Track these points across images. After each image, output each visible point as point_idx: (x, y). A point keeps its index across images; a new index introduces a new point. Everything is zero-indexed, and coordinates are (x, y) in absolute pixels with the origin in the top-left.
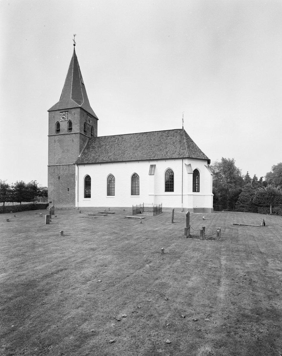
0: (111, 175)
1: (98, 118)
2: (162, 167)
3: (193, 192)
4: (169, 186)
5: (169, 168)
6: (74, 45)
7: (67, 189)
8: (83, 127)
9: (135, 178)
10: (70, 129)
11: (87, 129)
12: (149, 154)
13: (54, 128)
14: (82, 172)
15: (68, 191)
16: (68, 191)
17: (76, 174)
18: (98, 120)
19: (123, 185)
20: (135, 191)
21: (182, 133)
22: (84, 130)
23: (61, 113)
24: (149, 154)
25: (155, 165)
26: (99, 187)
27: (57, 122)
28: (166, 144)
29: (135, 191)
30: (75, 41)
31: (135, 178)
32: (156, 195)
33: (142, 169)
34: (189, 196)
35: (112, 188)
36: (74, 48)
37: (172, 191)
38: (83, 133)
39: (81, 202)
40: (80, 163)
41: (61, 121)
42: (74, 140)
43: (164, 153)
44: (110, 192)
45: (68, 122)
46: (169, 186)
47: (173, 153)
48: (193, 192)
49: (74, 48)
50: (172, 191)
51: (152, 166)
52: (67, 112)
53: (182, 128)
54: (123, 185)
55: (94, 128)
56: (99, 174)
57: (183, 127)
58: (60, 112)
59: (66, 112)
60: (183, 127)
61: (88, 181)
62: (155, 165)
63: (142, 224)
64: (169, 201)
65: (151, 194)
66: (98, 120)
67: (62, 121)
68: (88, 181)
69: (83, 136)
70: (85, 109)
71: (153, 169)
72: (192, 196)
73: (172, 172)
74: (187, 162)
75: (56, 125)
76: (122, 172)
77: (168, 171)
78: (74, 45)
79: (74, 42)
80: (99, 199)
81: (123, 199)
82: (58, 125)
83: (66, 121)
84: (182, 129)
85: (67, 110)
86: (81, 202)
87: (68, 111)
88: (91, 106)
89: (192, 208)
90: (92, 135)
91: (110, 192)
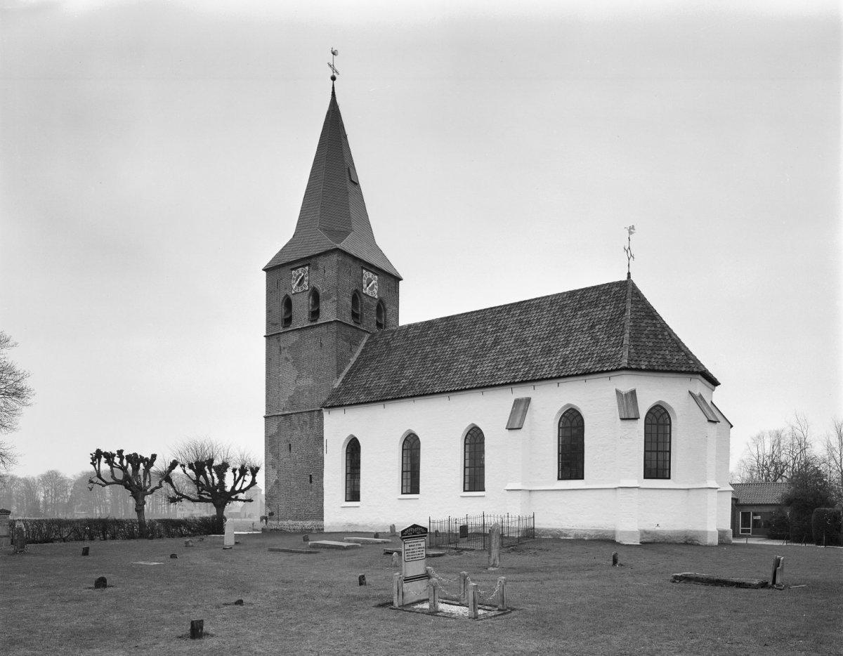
0: (412, 434)
1: (402, 274)
2: (548, 402)
3: (645, 478)
4: (571, 463)
5: (568, 405)
6: (333, 78)
8: (350, 303)
9: (474, 440)
10: (315, 314)
11: (362, 309)
12: (512, 368)
13: (280, 310)
14: (338, 427)
15: (311, 482)
16: (311, 482)
17: (467, 454)
18: (398, 279)
20: (474, 480)
22: (353, 312)
23: (293, 272)
24: (512, 368)
25: (528, 400)
26: (381, 467)
27: (284, 297)
28: (570, 331)
29: (474, 480)
30: (336, 67)
31: (474, 440)
32: (530, 491)
33: (488, 409)
35: (406, 471)
36: (333, 88)
37: (580, 476)
38: (348, 320)
40: (338, 402)
41: (293, 292)
42: (323, 342)
43: (556, 360)
44: (411, 481)
45: (310, 295)
46: (571, 463)
47: (582, 357)
48: (645, 478)
49: (333, 88)
50: (580, 476)
52: (307, 268)
53: (625, 278)
54: (443, 463)
55: (386, 305)
56: (379, 428)
57: (629, 274)
58: (292, 269)
59: (304, 266)
60: (629, 274)
62: (528, 400)
64: (569, 511)
65: (528, 487)
66: (401, 279)
67: (296, 293)
68: (353, 448)
69: (349, 330)
70: (352, 252)
73: (579, 415)
74: (625, 383)
75: (282, 303)
76: (440, 422)
78: (333, 78)
79: (330, 70)
80: (382, 507)
81: (443, 502)
82: (288, 303)
83: (305, 291)
84: (626, 281)
85: (308, 261)
86: (337, 513)
87: (309, 265)
88: (377, 244)
89: (636, 529)
90: (379, 325)
91: (411, 481)
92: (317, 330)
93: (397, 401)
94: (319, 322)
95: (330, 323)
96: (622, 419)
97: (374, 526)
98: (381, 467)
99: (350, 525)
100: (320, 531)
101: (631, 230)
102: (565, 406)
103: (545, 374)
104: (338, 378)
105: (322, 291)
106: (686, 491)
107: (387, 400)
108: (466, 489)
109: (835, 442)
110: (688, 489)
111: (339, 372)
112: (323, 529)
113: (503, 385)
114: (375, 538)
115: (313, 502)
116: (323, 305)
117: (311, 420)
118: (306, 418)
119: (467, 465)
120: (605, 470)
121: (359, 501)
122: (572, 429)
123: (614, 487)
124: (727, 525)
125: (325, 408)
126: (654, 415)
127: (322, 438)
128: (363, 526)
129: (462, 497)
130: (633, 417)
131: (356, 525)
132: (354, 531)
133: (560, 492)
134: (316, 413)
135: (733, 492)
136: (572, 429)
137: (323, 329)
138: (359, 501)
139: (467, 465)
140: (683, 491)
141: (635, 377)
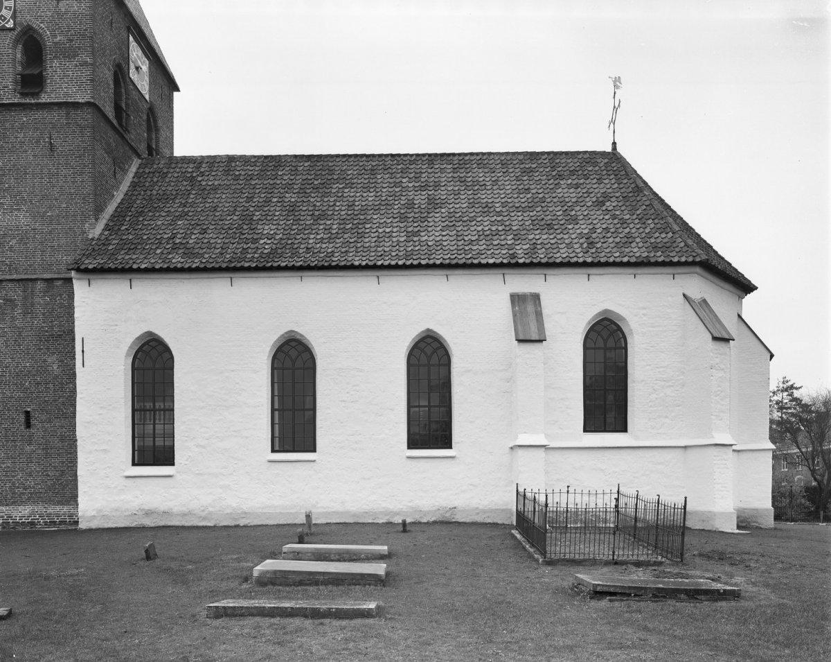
2: (572, 303)
4: (606, 404)
5: (606, 311)
7: (22, 418)
9: (429, 364)
14: (107, 319)
15: (28, 425)
16: (28, 425)
19: (363, 395)
20: (431, 427)
21: (611, 166)
26: (223, 401)
29: (431, 427)
31: (429, 364)
33: (470, 312)
34: (273, 464)
39: (109, 487)
46: (606, 404)
48: (585, 431)
51: (517, 299)
53: (609, 149)
54: (363, 395)
57: (614, 144)
60: (614, 144)
61: (152, 367)
63: (406, 534)
68: (152, 367)
71: (530, 308)
72: (541, 452)
76: (361, 327)
77: (599, 328)
80: (227, 472)
81: (363, 471)
86: (109, 487)
91: (294, 426)
92: (39, 115)
93: (175, 276)
94: (44, 99)
95: (76, 105)
96: (520, 341)
97: (210, 513)
98: (223, 401)
99: (148, 513)
100: (70, 528)
101: (617, 82)
102: (600, 314)
103: (105, 263)
104: (97, 220)
105: (50, 38)
106: (683, 449)
107: (382, 267)
108: (277, 448)
109: (828, 395)
110: (685, 447)
111: (99, 210)
112: (77, 523)
113: (686, 264)
114: (300, 542)
115: (33, 466)
116: (54, 68)
117: (25, 298)
118: (16, 293)
119: (276, 407)
120: (666, 417)
121: (173, 464)
122: (606, 346)
123: (683, 445)
124: (761, 500)
125: (78, 270)
126: (599, 333)
127: (71, 333)
128: (184, 515)
129: (408, 457)
130: (537, 338)
131: (164, 512)
132: (162, 524)
133: (660, 450)
134: (40, 286)
135: (774, 451)
136: (606, 346)
137: (55, 116)
138: (173, 464)
139: (276, 407)
140: (678, 451)
141: (268, 281)
